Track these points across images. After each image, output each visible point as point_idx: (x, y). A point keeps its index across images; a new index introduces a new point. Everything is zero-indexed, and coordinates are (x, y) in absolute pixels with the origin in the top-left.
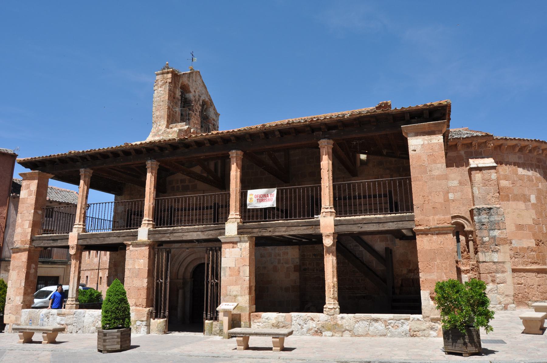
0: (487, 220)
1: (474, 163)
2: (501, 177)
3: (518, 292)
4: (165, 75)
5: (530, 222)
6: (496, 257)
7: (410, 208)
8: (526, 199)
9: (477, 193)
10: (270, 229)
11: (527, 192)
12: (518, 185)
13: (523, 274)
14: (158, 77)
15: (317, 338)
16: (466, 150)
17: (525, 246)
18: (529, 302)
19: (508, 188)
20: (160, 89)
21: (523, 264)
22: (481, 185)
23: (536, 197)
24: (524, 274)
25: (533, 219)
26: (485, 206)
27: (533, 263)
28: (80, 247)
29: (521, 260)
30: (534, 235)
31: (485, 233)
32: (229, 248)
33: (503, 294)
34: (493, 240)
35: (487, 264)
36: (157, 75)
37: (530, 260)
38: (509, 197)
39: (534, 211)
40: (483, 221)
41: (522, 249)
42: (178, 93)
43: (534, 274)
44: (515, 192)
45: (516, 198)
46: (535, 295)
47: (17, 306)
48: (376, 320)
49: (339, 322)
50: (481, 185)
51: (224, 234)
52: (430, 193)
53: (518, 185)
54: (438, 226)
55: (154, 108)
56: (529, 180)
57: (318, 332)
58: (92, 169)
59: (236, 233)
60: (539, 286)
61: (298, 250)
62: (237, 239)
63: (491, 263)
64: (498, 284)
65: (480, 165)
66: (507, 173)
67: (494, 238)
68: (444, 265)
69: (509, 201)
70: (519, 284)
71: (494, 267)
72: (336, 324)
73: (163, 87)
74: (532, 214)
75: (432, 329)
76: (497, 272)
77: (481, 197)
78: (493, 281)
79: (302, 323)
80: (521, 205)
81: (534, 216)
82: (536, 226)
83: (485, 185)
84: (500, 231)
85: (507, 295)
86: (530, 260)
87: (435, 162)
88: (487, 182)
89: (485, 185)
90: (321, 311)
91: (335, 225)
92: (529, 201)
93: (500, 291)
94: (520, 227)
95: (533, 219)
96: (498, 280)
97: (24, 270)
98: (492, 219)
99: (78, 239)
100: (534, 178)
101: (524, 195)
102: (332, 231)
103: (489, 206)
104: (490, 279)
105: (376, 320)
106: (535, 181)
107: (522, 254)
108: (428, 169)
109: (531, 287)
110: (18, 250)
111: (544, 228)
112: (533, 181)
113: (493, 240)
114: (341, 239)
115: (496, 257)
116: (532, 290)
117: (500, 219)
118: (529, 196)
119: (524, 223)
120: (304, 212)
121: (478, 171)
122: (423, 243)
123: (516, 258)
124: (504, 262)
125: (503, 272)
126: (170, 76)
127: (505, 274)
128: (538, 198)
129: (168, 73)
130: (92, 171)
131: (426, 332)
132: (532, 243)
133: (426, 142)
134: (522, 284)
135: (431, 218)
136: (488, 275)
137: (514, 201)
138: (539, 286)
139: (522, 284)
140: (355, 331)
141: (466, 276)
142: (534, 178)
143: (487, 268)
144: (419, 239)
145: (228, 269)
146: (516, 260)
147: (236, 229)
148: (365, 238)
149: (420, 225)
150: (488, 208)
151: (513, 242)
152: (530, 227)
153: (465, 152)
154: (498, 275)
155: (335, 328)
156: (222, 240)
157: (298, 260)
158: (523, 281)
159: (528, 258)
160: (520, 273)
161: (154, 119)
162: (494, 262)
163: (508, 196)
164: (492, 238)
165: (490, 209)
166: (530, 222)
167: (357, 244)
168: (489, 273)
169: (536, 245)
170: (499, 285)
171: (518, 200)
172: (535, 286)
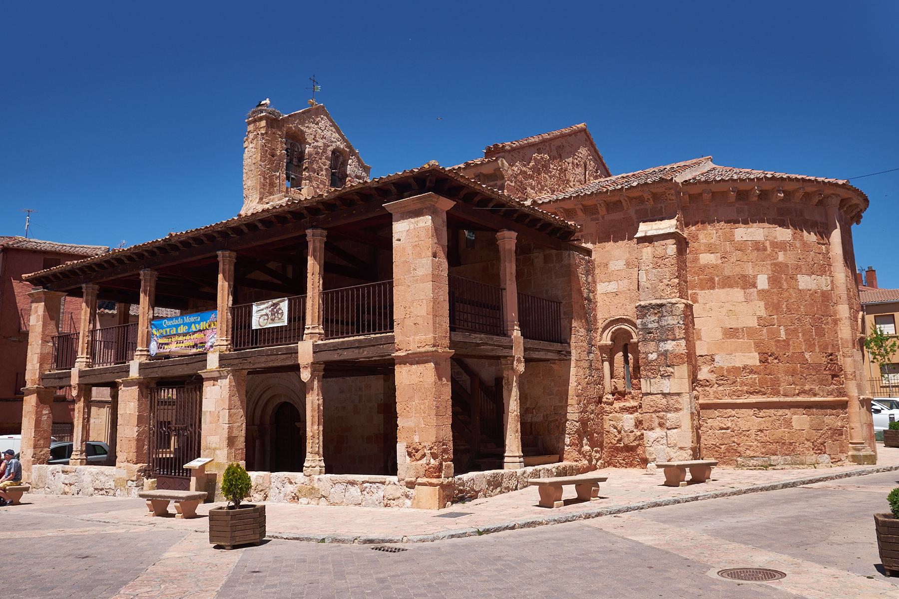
0: (656, 325)
1: (645, 229)
2: (702, 248)
3: (720, 442)
4: (258, 124)
5: (753, 323)
6: (667, 386)
7: (390, 325)
8: (747, 283)
9: (645, 280)
10: (249, 360)
11: (749, 270)
12: (733, 259)
13: (730, 412)
14: (251, 127)
15: (293, 505)
16: (638, 208)
17: (739, 364)
18: (739, 459)
19: (714, 267)
20: (251, 145)
21: (730, 396)
22: (651, 266)
23: (769, 278)
24: (733, 412)
25: (760, 318)
26: (654, 302)
27: (751, 393)
28: (84, 387)
29: (728, 389)
30: (757, 345)
31: (652, 346)
32: (210, 386)
33: (675, 445)
34: (663, 358)
35: (653, 397)
36: (249, 123)
37: (745, 388)
38: (714, 283)
39: (762, 304)
40: (650, 326)
41: (736, 370)
42: (281, 151)
43: (751, 412)
44: (727, 272)
45: (728, 283)
46: (751, 446)
47: (28, 461)
48: (353, 483)
49: (316, 486)
50: (651, 266)
51: (205, 367)
52: (413, 302)
53: (733, 259)
54: (419, 350)
55: (244, 175)
56: (758, 250)
57: (295, 498)
58: (97, 284)
59: (217, 365)
60: (761, 431)
61: (382, 382)
62: (216, 374)
63: (659, 396)
64: (668, 429)
65: (650, 233)
66: (712, 241)
67: (665, 354)
68: (422, 407)
69: (713, 288)
70: (721, 429)
71: (664, 401)
72: (313, 488)
73: (255, 142)
74: (760, 308)
75: (407, 496)
76: (668, 410)
77: (649, 286)
78: (661, 425)
79: (279, 485)
80: (737, 294)
81: (762, 312)
82: (765, 330)
83: (657, 266)
84: (674, 343)
85: (681, 448)
86: (745, 388)
87: (419, 255)
88: (660, 261)
89: (657, 266)
90: (299, 468)
91: (314, 353)
92: (754, 285)
93: (672, 441)
94: (731, 333)
95: (760, 318)
96: (668, 424)
97: (34, 417)
98: (664, 323)
99: (80, 377)
100: (768, 244)
101: (744, 277)
102: (311, 360)
103: (659, 302)
104: (657, 421)
105: (353, 483)
106: (769, 249)
107: (732, 377)
108: (413, 266)
109: (744, 433)
110: (31, 392)
111: (783, 332)
112: (765, 249)
113: (663, 358)
114: (330, 369)
115: (667, 386)
116: (746, 438)
117: (675, 322)
118: (755, 277)
119: (740, 326)
120: (380, 324)
121: (647, 244)
122: (404, 376)
123: (720, 385)
124: (679, 394)
125: (677, 410)
126: (263, 123)
127: (681, 413)
128: (774, 280)
129: (261, 119)
130: (97, 287)
131: (401, 501)
132: (753, 359)
133: (412, 226)
134: (727, 428)
135: (411, 339)
136: (654, 415)
137: (723, 288)
138: (761, 431)
139: (727, 428)
140: (330, 497)
141: (632, 416)
142: (768, 244)
143: (652, 403)
144: (398, 369)
145: (208, 414)
146: (721, 388)
147: (218, 360)
148: (469, 361)
149: (400, 350)
150: (658, 305)
151: (717, 358)
152: (750, 332)
153: (637, 211)
154: (669, 415)
155: (312, 492)
156: (204, 376)
157: (382, 396)
158: (729, 425)
159: (743, 384)
160: (725, 411)
161: (245, 192)
162: (665, 395)
163: (712, 280)
164: (662, 354)
165: (662, 305)
166: (753, 323)
167: (461, 370)
168: (655, 411)
169: (760, 361)
170: (668, 432)
171: (731, 287)
172: (753, 431)
